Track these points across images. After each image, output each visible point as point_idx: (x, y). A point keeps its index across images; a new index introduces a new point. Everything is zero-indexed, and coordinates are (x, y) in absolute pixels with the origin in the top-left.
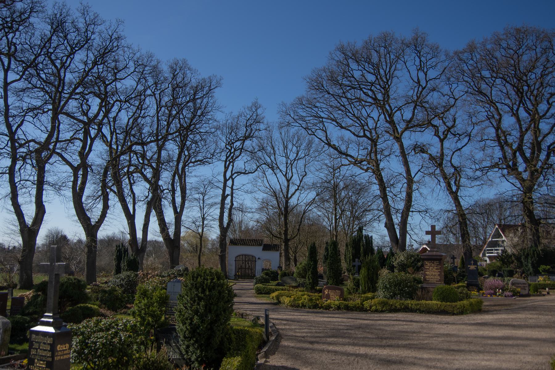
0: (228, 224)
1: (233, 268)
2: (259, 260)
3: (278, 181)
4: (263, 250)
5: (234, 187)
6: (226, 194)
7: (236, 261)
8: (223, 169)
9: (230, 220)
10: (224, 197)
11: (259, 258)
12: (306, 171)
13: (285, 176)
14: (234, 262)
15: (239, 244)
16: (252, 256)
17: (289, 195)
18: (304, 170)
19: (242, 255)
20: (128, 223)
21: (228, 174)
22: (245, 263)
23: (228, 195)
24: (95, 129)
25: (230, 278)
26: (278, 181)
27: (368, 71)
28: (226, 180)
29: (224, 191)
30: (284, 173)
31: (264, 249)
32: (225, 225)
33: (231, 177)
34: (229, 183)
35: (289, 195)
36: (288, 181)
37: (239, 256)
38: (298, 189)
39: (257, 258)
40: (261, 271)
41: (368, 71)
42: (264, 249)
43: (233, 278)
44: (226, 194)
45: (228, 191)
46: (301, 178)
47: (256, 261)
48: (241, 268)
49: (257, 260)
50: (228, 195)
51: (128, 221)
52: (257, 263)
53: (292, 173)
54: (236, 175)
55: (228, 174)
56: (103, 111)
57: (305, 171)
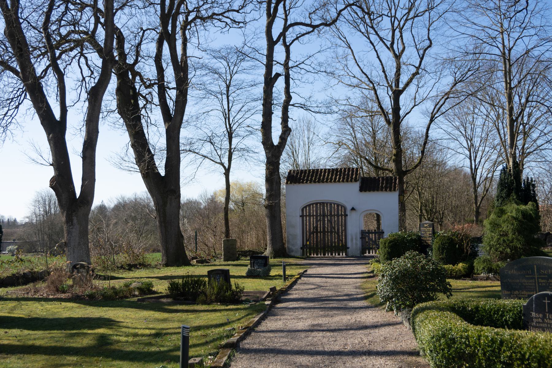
0: (283, 139)
1: (298, 231)
2: (354, 212)
3: (378, 57)
4: (361, 190)
5: (291, 64)
6: (274, 73)
7: (302, 216)
8: (264, 20)
9: (286, 131)
10: (270, 81)
11: (353, 209)
12: (432, 38)
13: (391, 48)
14: (299, 220)
15: (307, 180)
16: (338, 205)
17: (401, 86)
18: (426, 37)
19: (317, 204)
20: (49, 140)
21: (277, 30)
22: (324, 221)
23: (278, 75)
24: (182, 150)
25: (292, 254)
26: (378, 57)
27: (17, 299)
28: (271, 44)
29: (269, 66)
30: (389, 44)
31: (362, 189)
32: (276, 141)
33: (283, 34)
34: (279, 53)
35: (401, 86)
36: (398, 57)
37: (309, 205)
38: (417, 73)
39: (349, 208)
40: (359, 236)
41: (17, 299)
42: (362, 189)
43: (299, 253)
44: (274, 73)
45: (277, 69)
46: (421, 52)
47: (346, 215)
48: (316, 230)
49: (348, 212)
50: (278, 75)
51: (48, 134)
52: (348, 218)
53: (403, 44)
54: (299, 29)
55: (277, 28)
56: (114, 73)
57: (429, 39)
